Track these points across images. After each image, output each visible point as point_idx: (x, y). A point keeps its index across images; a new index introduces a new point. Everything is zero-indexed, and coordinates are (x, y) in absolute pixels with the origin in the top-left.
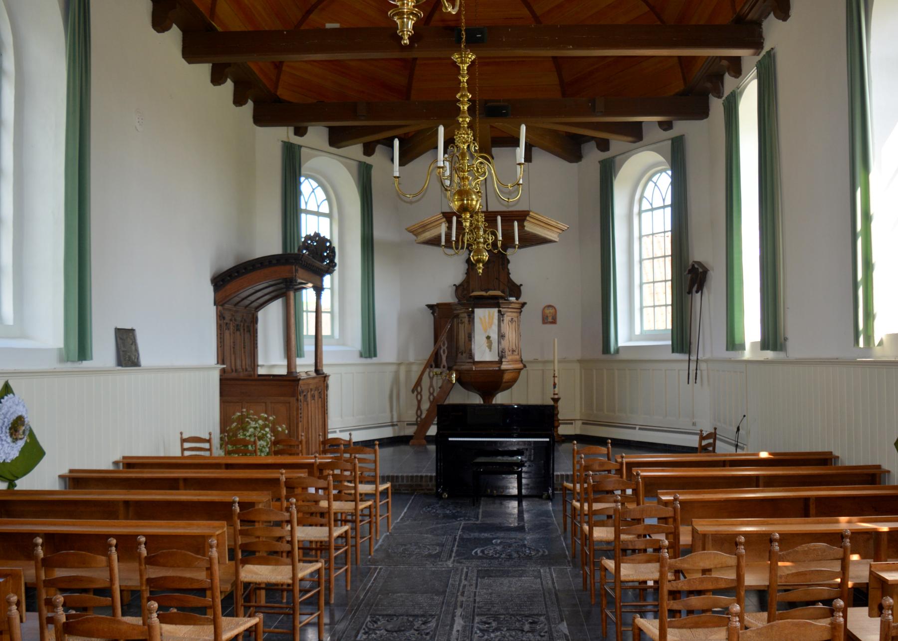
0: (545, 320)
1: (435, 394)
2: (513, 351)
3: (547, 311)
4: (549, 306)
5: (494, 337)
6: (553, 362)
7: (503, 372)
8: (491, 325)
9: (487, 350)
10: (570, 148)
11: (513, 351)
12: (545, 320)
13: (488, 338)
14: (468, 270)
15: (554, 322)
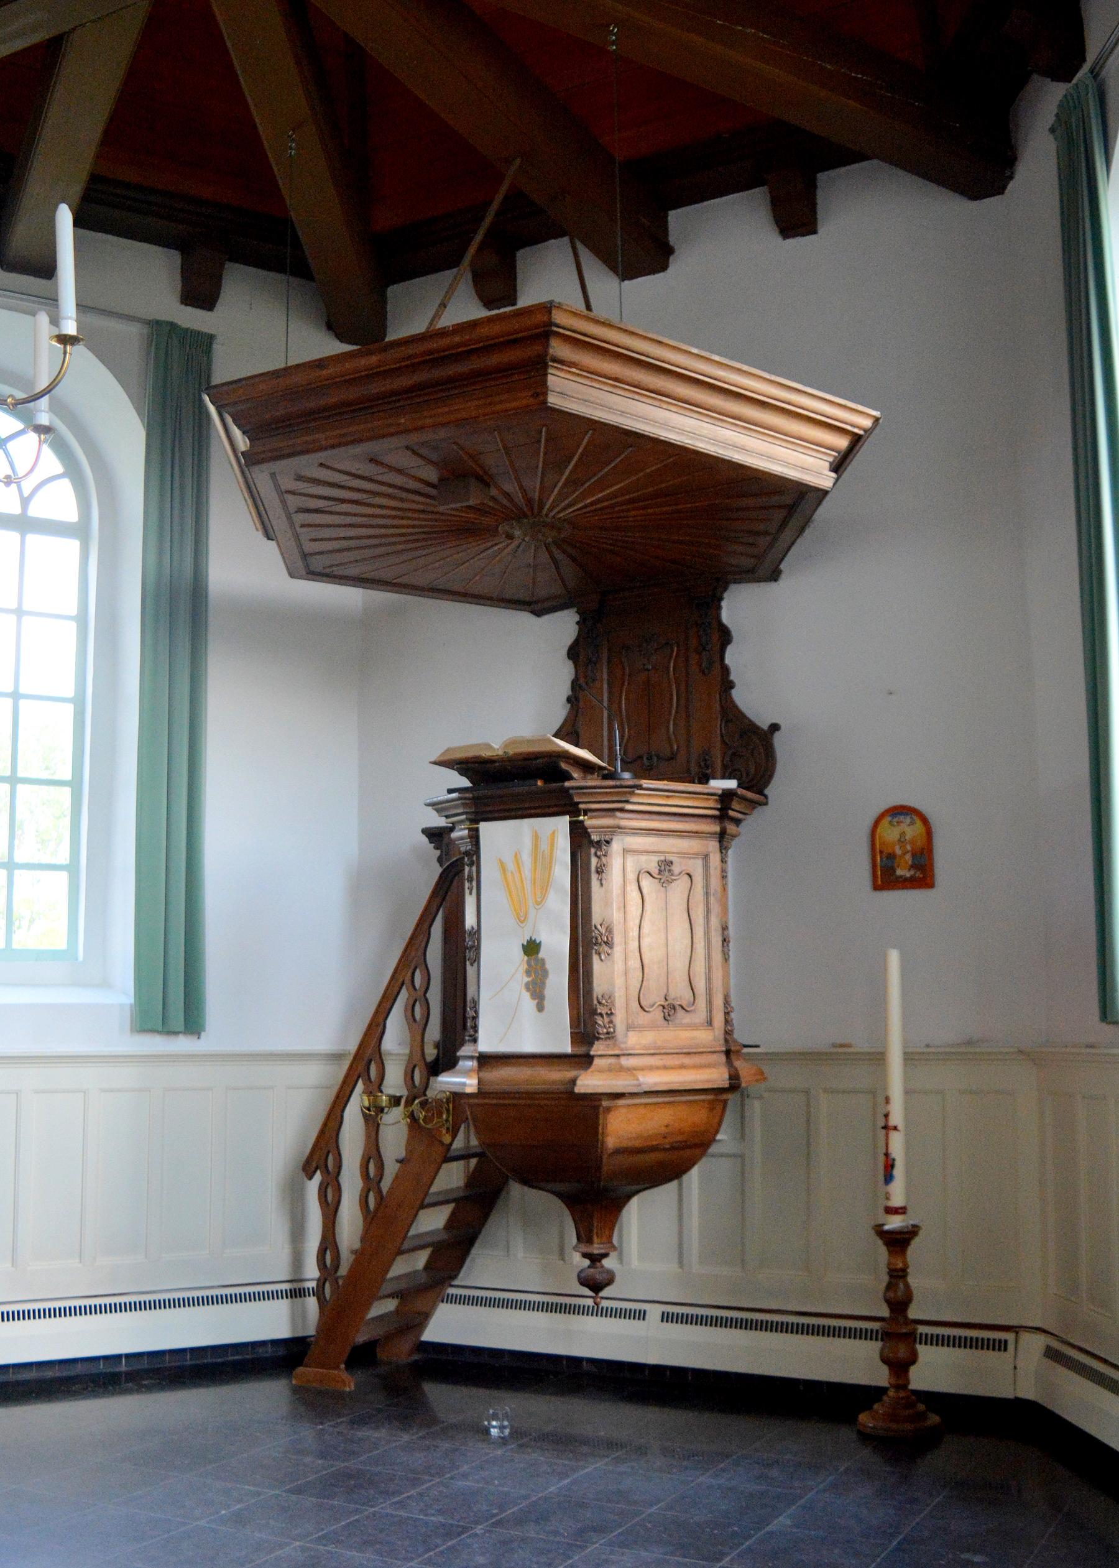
0: (886, 876)
1: (386, 1185)
2: (670, 1010)
3: (890, 833)
4: (899, 811)
5: (557, 943)
6: (878, 1058)
7: (592, 1106)
8: (544, 885)
9: (528, 1003)
10: (976, 164)
11: (670, 1010)
12: (886, 876)
13: (531, 948)
14: (575, 685)
15: (922, 875)
